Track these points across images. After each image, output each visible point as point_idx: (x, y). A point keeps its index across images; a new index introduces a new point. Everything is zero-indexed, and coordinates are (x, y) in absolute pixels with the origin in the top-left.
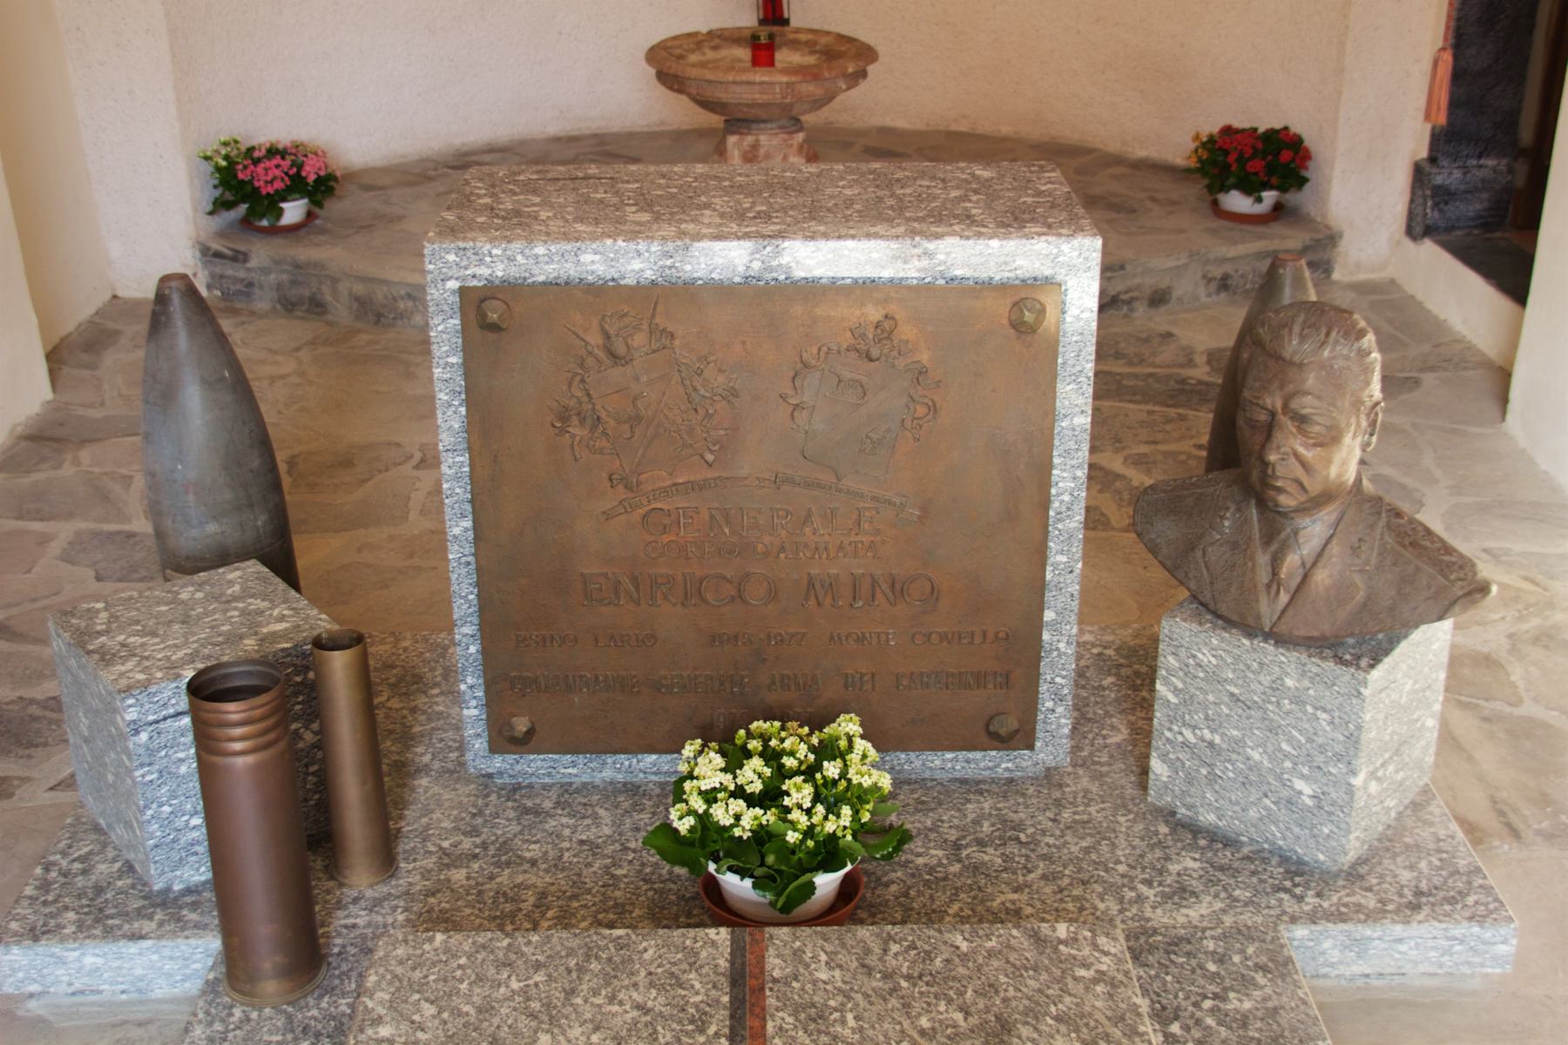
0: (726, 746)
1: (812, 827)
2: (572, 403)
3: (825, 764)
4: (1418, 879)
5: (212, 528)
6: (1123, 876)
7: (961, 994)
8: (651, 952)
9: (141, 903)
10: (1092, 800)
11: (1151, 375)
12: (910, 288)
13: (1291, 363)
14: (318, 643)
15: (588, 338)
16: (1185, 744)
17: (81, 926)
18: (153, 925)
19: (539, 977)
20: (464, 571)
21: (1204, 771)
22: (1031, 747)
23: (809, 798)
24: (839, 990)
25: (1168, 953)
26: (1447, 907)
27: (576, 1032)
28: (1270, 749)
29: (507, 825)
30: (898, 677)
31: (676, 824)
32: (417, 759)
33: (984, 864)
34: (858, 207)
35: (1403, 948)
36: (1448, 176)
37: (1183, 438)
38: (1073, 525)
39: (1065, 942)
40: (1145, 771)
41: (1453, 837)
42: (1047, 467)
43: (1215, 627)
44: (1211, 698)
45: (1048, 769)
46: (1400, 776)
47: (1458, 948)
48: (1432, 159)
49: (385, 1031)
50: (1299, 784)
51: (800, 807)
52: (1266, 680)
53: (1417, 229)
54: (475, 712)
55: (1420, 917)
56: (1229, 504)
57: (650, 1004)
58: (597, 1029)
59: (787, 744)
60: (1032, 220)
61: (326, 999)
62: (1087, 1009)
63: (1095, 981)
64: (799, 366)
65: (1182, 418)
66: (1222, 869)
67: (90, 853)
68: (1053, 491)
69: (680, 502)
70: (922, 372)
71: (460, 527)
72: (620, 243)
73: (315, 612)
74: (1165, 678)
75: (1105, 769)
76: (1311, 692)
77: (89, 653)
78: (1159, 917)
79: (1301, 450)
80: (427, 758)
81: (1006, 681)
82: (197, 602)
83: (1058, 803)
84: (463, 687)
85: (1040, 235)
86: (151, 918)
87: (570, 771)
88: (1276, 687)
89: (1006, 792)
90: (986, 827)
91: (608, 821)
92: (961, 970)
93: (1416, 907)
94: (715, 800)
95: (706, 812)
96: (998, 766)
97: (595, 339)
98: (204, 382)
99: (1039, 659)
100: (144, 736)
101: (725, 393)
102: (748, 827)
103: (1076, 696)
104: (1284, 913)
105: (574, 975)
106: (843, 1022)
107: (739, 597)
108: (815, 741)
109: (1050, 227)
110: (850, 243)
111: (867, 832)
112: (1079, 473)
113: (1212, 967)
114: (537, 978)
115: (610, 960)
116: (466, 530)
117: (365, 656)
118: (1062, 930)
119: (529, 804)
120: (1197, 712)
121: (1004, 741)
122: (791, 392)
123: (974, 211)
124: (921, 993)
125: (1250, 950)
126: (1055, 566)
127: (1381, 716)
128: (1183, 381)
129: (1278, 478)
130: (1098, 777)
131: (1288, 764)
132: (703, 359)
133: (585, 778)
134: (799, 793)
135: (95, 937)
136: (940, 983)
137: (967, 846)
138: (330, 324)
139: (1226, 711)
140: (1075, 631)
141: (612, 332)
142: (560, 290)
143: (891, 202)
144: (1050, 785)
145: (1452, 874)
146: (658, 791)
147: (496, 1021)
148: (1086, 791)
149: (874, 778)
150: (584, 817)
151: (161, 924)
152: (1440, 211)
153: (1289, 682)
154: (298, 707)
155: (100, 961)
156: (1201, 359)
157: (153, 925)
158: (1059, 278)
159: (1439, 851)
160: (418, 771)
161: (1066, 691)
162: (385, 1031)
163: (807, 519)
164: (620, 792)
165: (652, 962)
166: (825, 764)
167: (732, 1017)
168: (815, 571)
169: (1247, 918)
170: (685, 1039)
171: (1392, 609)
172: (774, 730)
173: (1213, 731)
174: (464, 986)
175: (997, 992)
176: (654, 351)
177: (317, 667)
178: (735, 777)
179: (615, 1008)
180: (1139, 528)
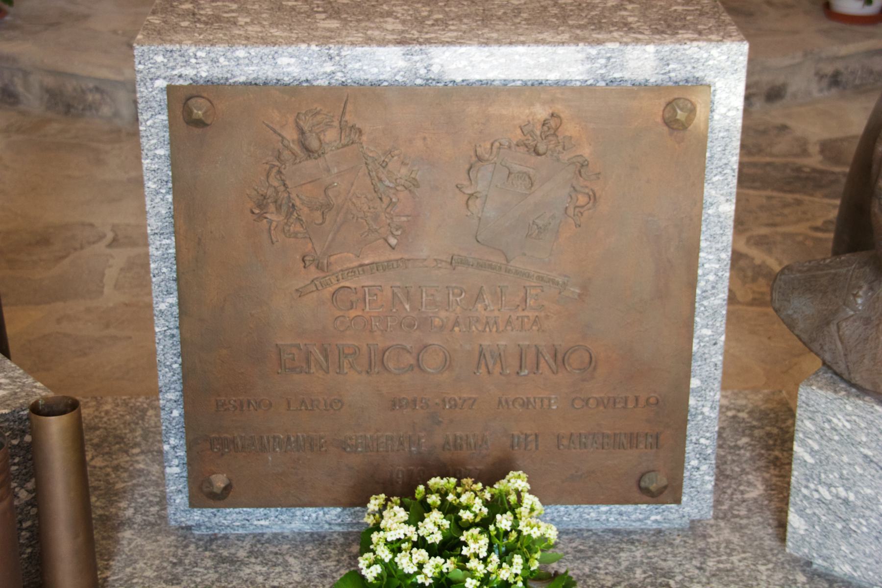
0: (407, 500)
1: (488, 574)
2: (270, 192)
3: (498, 516)
10: (733, 550)
11: (769, 164)
12: (573, 89)
14: (36, 409)
15: (284, 134)
16: (821, 501)
20: (169, 342)
21: (839, 526)
22: (678, 501)
23: (485, 548)
30: (559, 437)
31: (363, 572)
32: (120, 513)
34: (525, 15)
37: (799, 221)
38: (717, 302)
40: (782, 525)
42: (697, 249)
43: (849, 395)
45: (692, 521)
51: (477, 556)
54: (177, 470)
56: (862, 283)
59: (464, 499)
60: (684, 27)
64: (474, 159)
65: (799, 203)
68: (700, 272)
69: (366, 281)
70: (584, 165)
71: (166, 303)
72: (314, 47)
73: (31, 380)
74: (802, 441)
75: (744, 522)
80: (130, 512)
81: (656, 442)
83: (703, 552)
84: (166, 447)
85: (692, 40)
87: (263, 522)
89: (655, 542)
90: (639, 574)
91: (297, 568)
94: (400, 550)
95: (392, 560)
96: (648, 518)
97: (291, 134)
99: (685, 422)
101: (407, 184)
102: (430, 575)
103: (719, 457)
107: (418, 365)
108: (487, 496)
109: (700, 33)
110: (521, 49)
111: (535, 579)
116: (171, 305)
117: (79, 419)
119: (225, 553)
120: (832, 472)
121: (653, 496)
122: (466, 183)
123: (630, 19)
126: (701, 338)
128: (799, 169)
130: (738, 528)
132: (389, 153)
133: (276, 529)
134: (475, 543)
138: (23, 113)
139: (859, 470)
140: (718, 397)
141: (306, 128)
142: (259, 90)
143: (555, 11)
144: (695, 536)
146: (341, 540)
148: (728, 542)
149: (543, 530)
154: (14, 468)
156: (814, 149)
158: (708, 80)
160: (122, 524)
161: (709, 451)
163: (479, 297)
164: (308, 542)
166: (498, 516)
168: (486, 343)
172: (451, 486)
173: (847, 489)
176: (344, 146)
177: (34, 431)
178: (417, 529)
180: (777, 305)
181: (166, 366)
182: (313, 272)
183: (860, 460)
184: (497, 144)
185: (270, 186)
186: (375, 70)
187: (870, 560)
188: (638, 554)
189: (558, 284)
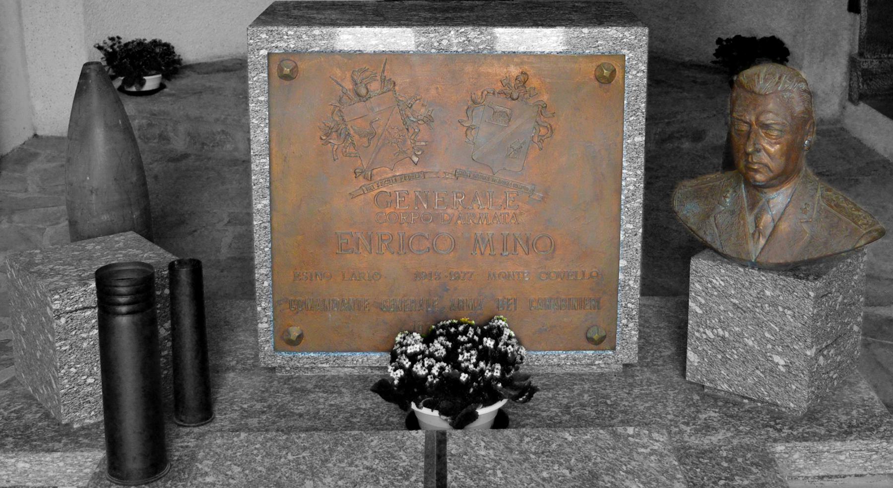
4: (851, 419)
5: (105, 217)
6: (671, 421)
7: (568, 461)
8: (375, 442)
9: (53, 434)
13: (760, 95)
15: (343, 84)
16: (708, 340)
17: (16, 445)
18: (61, 445)
19: (306, 454)
24: (493, 459)
25: (698, 458)
26: (868, 433)
27: (328, 480)
28: (758, 337)
29: (284, 398)
33: (583, 415)
35: (842, 457)
36: (871, 63)
39: (633, 436)
41: (872, 399)
43: (722, 262)
44: (722, 308)
46: (839, 358)
47: (875, 457)
48: (861, 54)
49: (209, 479)
50: (777, 359)
52: (754, 293)
53: (856, 96)
54: (266, 325)
55: (852, 438)
57: (374, 466)
58: (341, 479)
61: (169, 482)
62: (645, 467)
63: (651, 454)
64: (470, 103)
66: (732, 416)
67: (22, 408)
68: (624, 183)
69: (397, 188)
74: (694, 298)
76: (781, 298)
77: (31, 273)
78: (694, 441)
79: (767, 147)
81: (598, 305)
82: (96, 251)
83: (631, 385)
86: (60, 442)
87: (324, 365)
88: (761, 297)
92: (568, 450)
93: (851, 433)
97: (348, 85)
98: (106, 125)
100: (63, 320)
101: (425, 119)
104: (769, 437)
105: (327, 453)
106: (495, 475)
107: (433, 249)
112: (639, 172)
113: (725, 465)
114: (304, 454)
115: (350, 445)
116: (265, 206)
118: (630, 430)
119: (299, 386)
122: (465, 119)
124: (543, 461)
125: (749, 455)
126: (626, 231)
127: (823, 313)
129: (754, 163)
131: (769, 346)
133: (334, 372)
135: (25, 450)
136: (556, 456)
137: (573, 407)
141: (358, 82)
145: (871, 417)
147: (279, 475)
148: (649, 379)
150: (333, 393)
151: (65, 445)
152: (868, 84)
153: (768, 293)
155: (28, 466)
157: (61, 445)
159: (864, 406)
162: (209, 479)
165: (376, 447)
167: (425, 472)
169: (747, 440)
170: (396, 483)
171: (826, 243)
174: (259, 458)
175: (590, 460)
176: (383, 93)
179: (353, 468)
181: (261, 250)
182: (362, 182)
183: (731, 308)
184: (486, 92)
185: (334, 120)
186: (404, 43)
187: (740, 379)
188: (586, 387)
189: (527, 189)
